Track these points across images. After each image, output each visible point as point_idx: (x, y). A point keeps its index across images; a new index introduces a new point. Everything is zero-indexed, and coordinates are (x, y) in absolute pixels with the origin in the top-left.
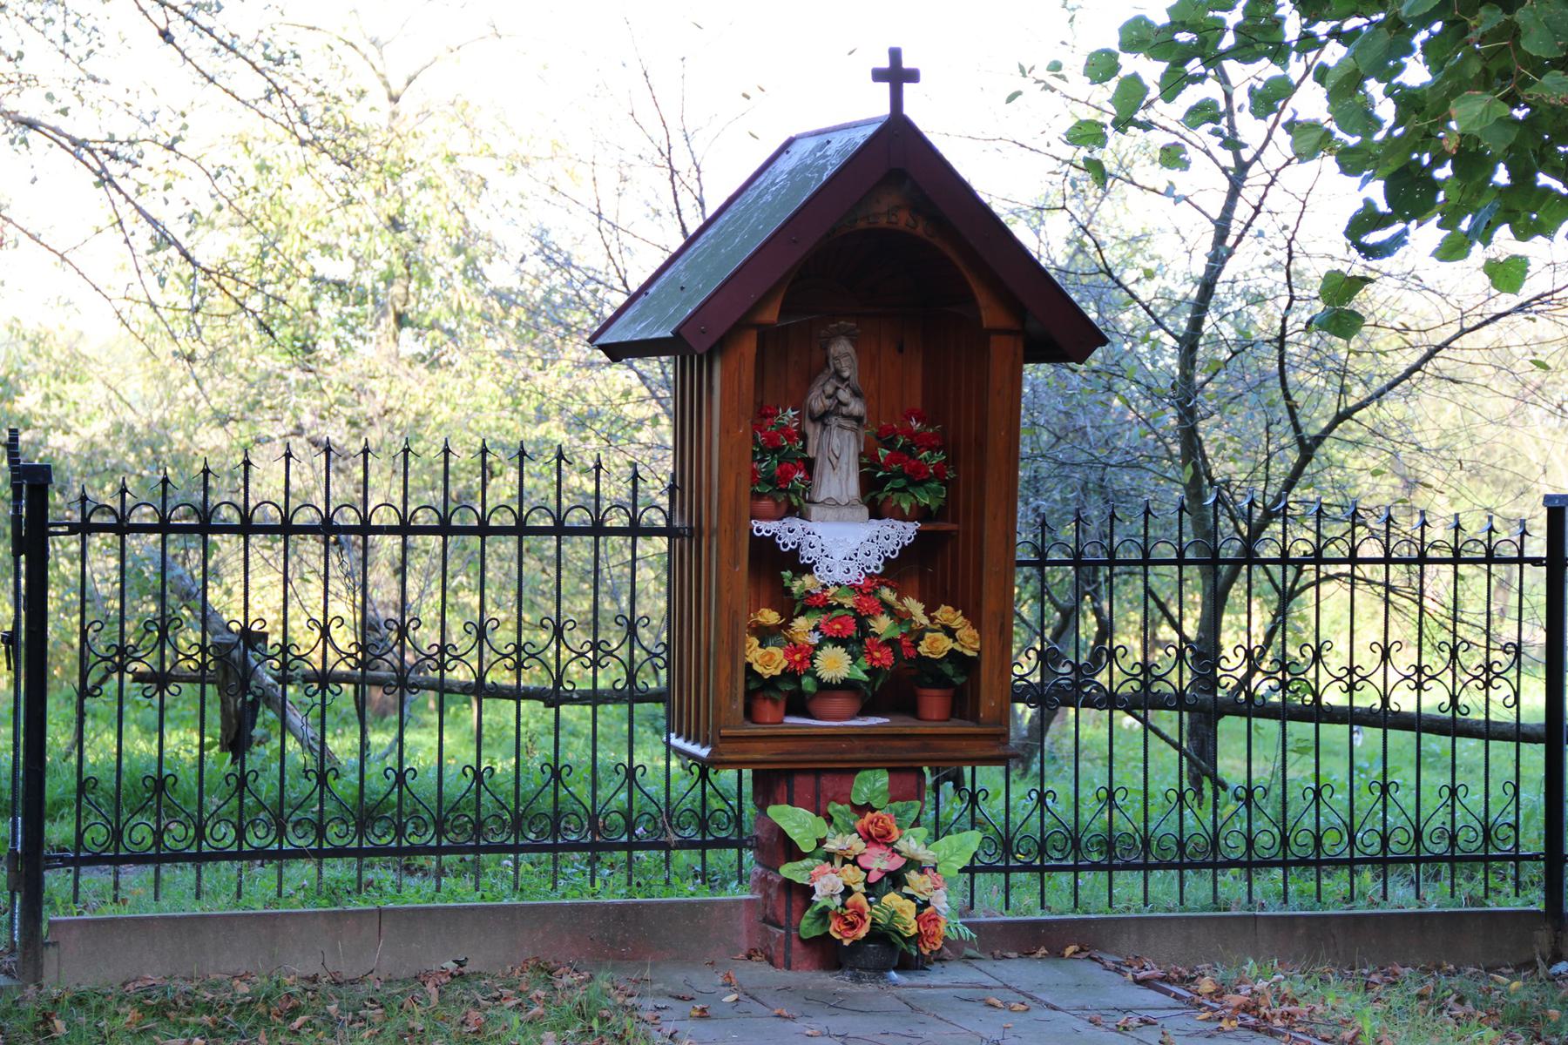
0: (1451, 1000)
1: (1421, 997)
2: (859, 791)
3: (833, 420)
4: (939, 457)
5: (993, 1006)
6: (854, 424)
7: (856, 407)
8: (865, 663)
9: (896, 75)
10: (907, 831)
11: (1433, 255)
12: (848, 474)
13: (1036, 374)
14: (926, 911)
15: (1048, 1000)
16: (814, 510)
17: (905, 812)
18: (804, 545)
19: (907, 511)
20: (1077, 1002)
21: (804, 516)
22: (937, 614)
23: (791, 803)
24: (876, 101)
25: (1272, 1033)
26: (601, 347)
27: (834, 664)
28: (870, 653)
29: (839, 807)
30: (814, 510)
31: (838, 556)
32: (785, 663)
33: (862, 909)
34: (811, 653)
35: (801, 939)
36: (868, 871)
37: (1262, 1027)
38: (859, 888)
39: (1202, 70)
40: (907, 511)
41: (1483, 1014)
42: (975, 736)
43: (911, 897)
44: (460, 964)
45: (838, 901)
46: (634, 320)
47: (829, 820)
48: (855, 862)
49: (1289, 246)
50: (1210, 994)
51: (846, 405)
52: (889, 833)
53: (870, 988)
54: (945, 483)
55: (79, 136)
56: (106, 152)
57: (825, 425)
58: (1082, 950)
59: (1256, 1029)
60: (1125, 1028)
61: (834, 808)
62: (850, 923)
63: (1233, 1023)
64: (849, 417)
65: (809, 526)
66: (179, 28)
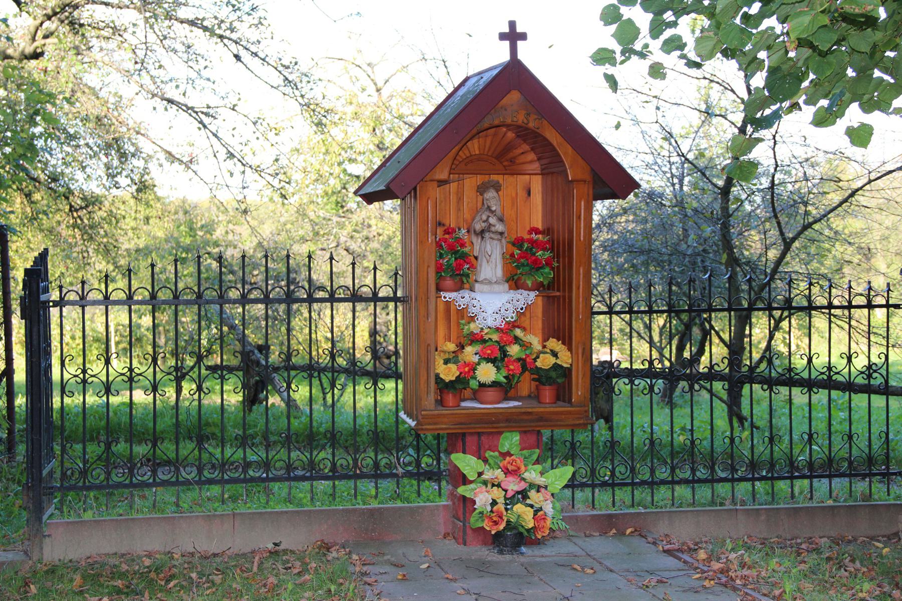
0: (847, 560)
1: (829, 559)
2: (503, 445)
3: (487, 235)
4: (548, 254)
5: (575, 569)
6: (499, 237)
7: (500, 227)
8: (504, 373)
9: (513, 36)
10: (530, 467)
11: (811, 123)
12: (496, 266)
13: (601, 208)
14: (540, 514)
15: (608, 564)
16: (477, 286)
17: (530, 455)
18: (470, 305)
19: (530, 285)
20: (625, 566)
21: (472, 290)
22: (547, 343)
23: (464, 452)
24: (501, 54)
25: (735, 589)
26: (361, 196)
27: (487, 373)
28: (507, 366)
29: (492, 453)
30: (477, 286)
31: (490, 312)
32: (458, 373)
33: (502, 513)
34: (473, 368)
35: (473, 530)
36: (506, 491)
37: (729, 585)
38: (501, 500)
39: (673, 18)
40: (530, 285)
41: (865, 570)
42: (570, 413)
43: (532, 506)
44: (276, 544)
45: (489, 508)
46: (375, 182)
47: (486, 461)
48: (499, 486)
49: (774, 137)
50: (704, 560)
51: (494, 226)
52: (519, 468)
53: (508, 557)
54: (552, 269)
55: (190, 105)
56: (202, 113)
57: (483, 238)
58: (636, 530)
59: (725, 585)
60: (647, 587)
61: (488, 454)
62: (495, 521)
63: (712, 582)
64: (497, 233)
65: (473, 295)
66: (243, 54)
